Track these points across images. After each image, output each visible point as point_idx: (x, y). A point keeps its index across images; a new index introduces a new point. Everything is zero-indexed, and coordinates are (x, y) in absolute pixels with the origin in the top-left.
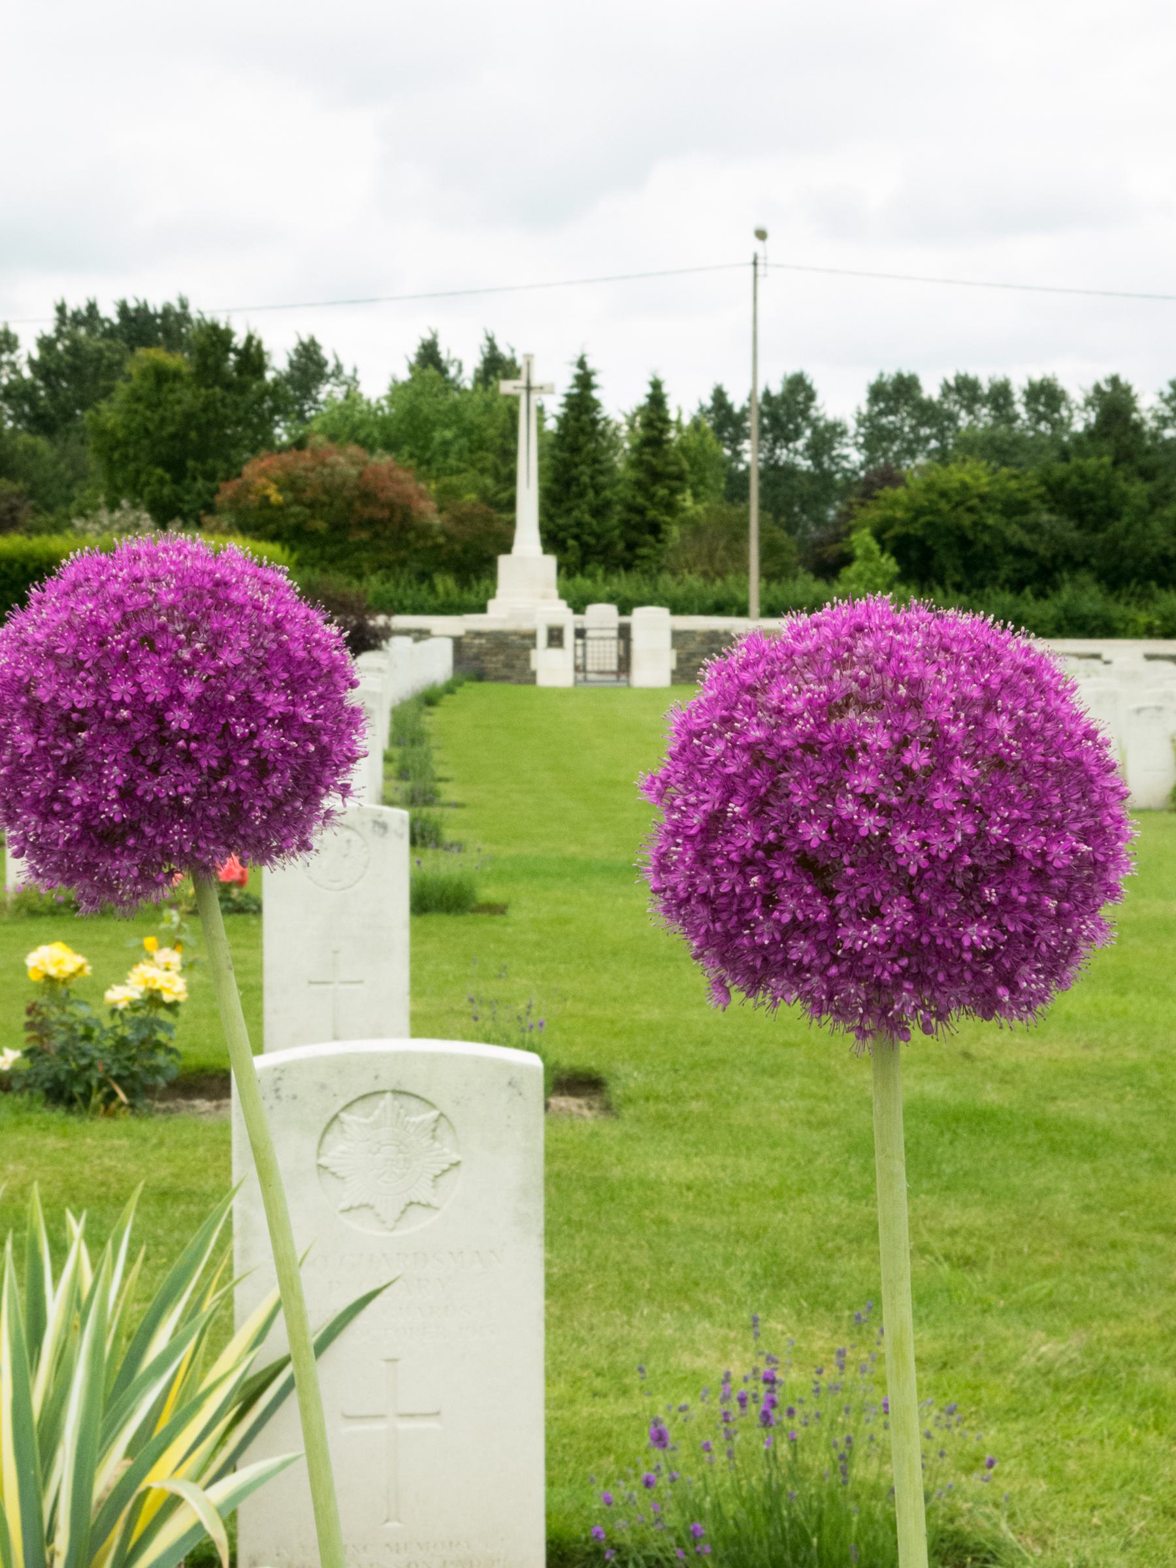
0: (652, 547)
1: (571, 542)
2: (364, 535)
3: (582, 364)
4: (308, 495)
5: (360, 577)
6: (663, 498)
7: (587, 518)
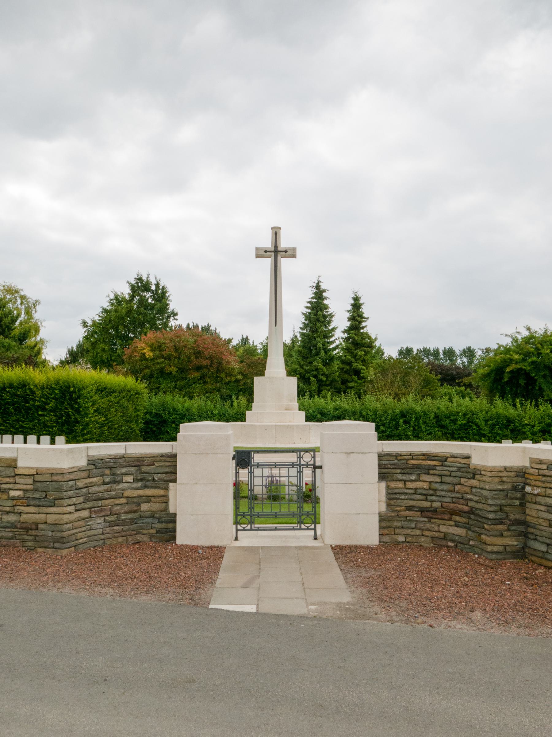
0: (356, 382)
1: (312, 379)
2: (197, 375)
3: (318, 287)
4: (166, 353)
5: (191, 398)
6: (361, 357)
7: (321, 365)
